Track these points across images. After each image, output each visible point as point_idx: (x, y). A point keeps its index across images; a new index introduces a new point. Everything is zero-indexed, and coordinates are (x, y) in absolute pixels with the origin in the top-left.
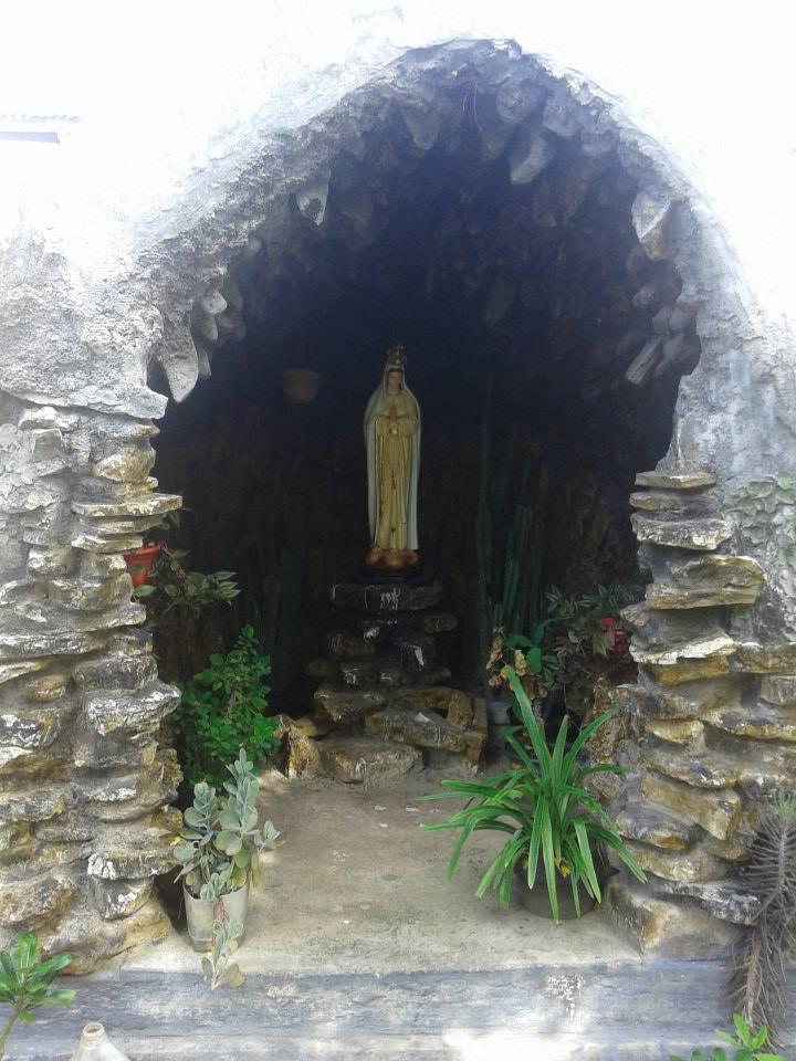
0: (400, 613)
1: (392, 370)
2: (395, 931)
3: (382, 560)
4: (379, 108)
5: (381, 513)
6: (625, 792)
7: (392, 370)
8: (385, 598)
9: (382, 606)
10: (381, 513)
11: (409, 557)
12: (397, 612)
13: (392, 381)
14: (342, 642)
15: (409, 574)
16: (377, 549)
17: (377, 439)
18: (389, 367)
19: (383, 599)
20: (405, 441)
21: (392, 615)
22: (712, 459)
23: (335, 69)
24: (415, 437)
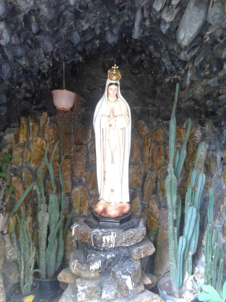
0: (117, 248)
1: (111, 84)
2: (105, 262)
3: (105, 210)
4: (21, 146)
5: (104, 178)
6: (152, 68)
7: (111, 84)
8: (106, 240)
9: (103, 246)
10: (104, 178)
11: (123, 208)
12: (115, 248)
13: (111, 92)
14: (78, 266)
15: (125, 220)
16: (101, 202)
17: (102, 130)
18: (109, 81)
19: (104, 241)
20: (121, 132)
21: (111, 250)
22: (43, 31)
23: (222, 48)
24: (126, 129)
